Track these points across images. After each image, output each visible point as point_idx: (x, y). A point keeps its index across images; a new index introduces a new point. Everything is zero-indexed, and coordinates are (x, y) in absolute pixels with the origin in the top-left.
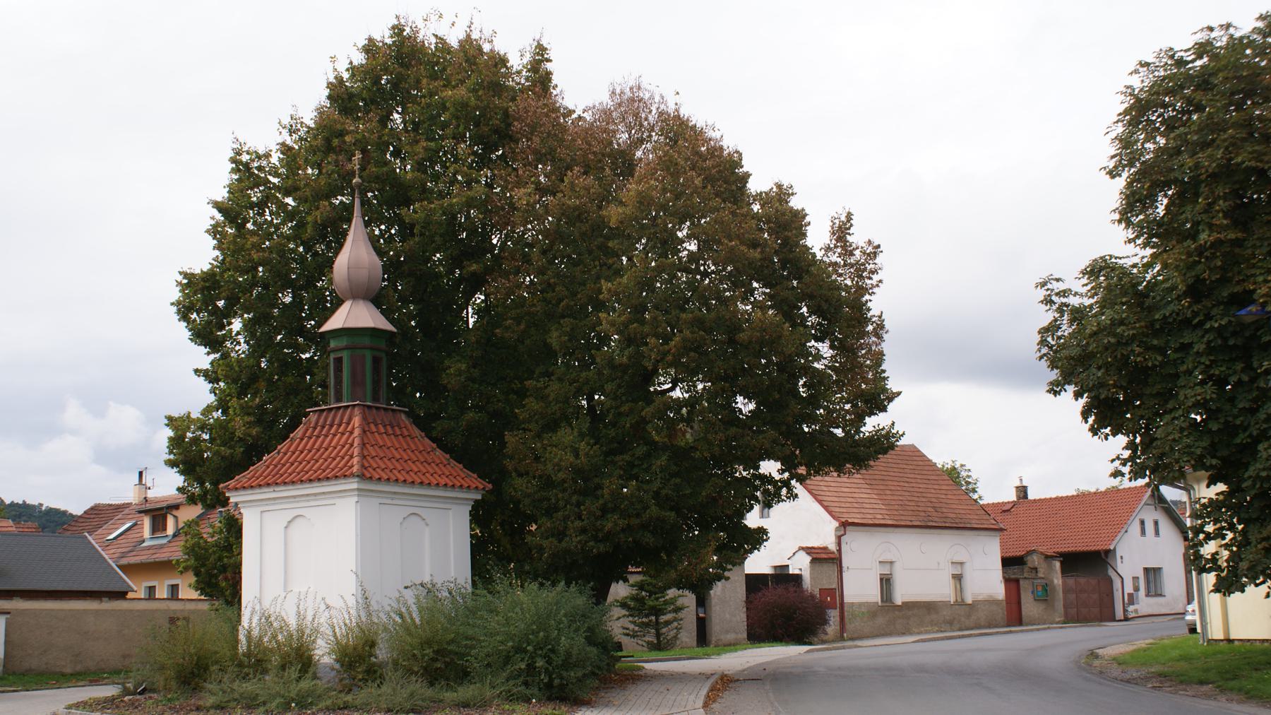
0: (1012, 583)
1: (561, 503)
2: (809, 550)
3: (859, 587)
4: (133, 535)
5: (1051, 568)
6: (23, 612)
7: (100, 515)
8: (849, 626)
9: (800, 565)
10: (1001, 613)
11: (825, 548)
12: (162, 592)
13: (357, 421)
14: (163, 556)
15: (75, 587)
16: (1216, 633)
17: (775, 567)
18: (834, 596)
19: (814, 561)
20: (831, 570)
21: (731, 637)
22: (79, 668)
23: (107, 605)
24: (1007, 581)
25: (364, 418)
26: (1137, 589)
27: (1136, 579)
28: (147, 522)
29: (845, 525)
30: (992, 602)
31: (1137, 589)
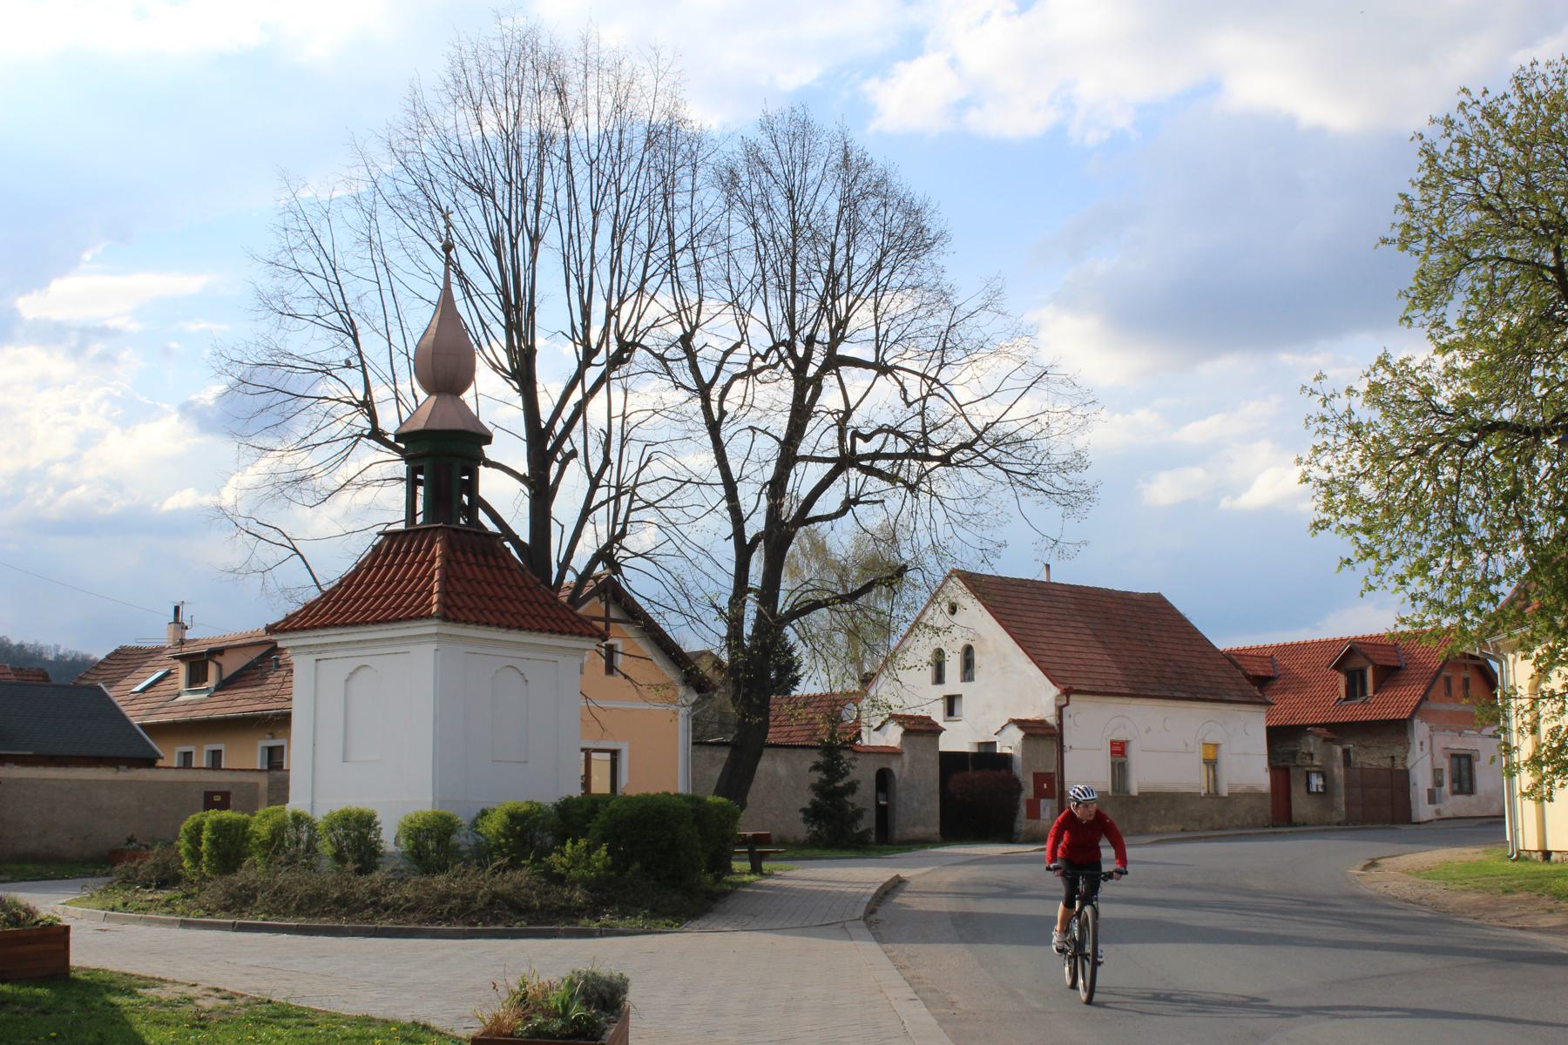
3: (1085, 774)
5: (1330, 756)
9: (1010, 743)
11: (1043, 722)
18: (1050, 784)
20: (1049, 748)
21: (919, 831)
24: (1274, 768)
26: (1439, 784)
29: (1067, 692)
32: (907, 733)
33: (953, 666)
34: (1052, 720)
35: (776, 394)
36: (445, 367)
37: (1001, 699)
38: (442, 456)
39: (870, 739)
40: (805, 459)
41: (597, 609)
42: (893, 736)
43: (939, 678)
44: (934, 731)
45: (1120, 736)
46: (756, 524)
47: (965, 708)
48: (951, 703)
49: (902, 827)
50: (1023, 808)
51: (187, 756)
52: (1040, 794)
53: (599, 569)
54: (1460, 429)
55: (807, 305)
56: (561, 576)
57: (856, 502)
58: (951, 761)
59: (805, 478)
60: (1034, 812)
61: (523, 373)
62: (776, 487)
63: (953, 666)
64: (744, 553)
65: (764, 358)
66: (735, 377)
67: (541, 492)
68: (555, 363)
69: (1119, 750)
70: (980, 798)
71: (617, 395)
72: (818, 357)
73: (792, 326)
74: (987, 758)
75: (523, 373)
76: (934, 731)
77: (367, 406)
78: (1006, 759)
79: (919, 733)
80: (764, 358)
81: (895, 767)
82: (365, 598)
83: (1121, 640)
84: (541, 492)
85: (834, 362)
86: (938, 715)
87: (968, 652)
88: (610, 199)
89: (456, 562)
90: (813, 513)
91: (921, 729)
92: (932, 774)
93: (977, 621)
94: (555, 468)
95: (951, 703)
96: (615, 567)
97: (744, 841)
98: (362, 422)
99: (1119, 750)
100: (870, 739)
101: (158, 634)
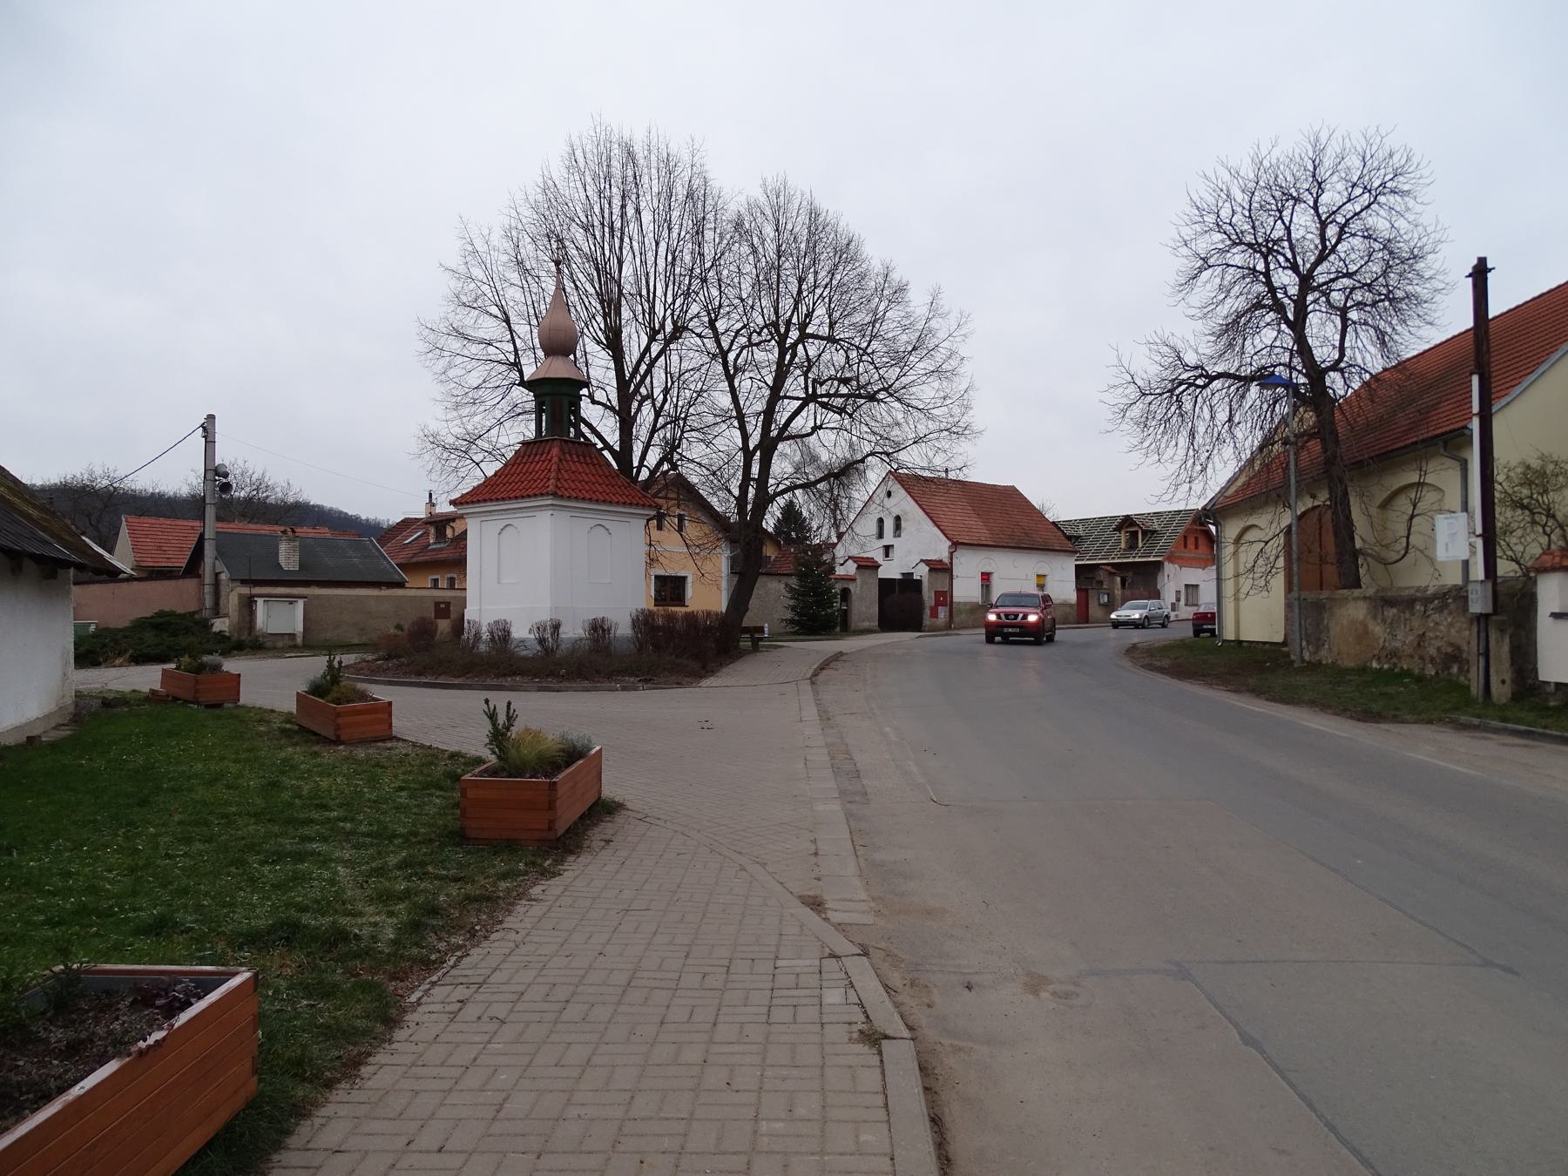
0: (1081, 590)
1: (1514, 525)
2: (927, 562)
3: (966, 589)
4: (422, 541)
5: (1113, 582)
6: (318, 596)
7: (407, 524)
8: (956, 619)
9: (921, 572)
10: (1074, 612)
11: (941, 561)
12: (443, 583)
13: (555, 451)
14: (442, 556)
15: (370, 579)
16: (1229, 634)
17: (1542, 457)
18: (944, 597)
19: (931, 570)
20: (945, 577)
21: (866, 624)
22: (364, 639)
23: (385, 592)
24: (1078, 590)
25: (561, 449)
26: (1178, 600)
27: (1178, 592)
28: (432, 530)
29: (956, 545)
30: (1065, 604)
31: (1178, 600)
32: (859, 567)
33: (889, 525)
34: (946, 560)
35: (767, 356)
36: (559, 345)
37: (915, 547)
38: (557, 398)
39: (840, 571)
40: (786, 397)
41: (667, 496)
42: (851, 568)
43: (880, 535)
44: (877, 567)
45: (987, 569)
46: (753, 442)
47: (895, 554)
48: (887, 549)
49: (856, 620)
50: (927, 611)
51: (436, 581)
52: (938, 603)
53: (666, 467)
54: (1197, 378)
55: (786, 304)
56: (639, 472)
57: (820, 427)
58: (886, 585)
59: (786, 408)
60: (934, 614)
61: (614, 344)
62: (769, 413)
63: (889, 525)
64: (748, 455)
65: (759, 334)
66: (743, 348)
67: (626, 423)
68: (634, 340)
69: (986, 577)
70: (903, 605)
71: (675, 358)
72: (794, 334)
73: (776, 312)
74: (909, 584)
75: (614, 344)
76: (877, 567)
77: (516, 365)
78: (919, 582)
79: (866, 567)
80: (759, 334)
81: (852, 587)
82: (512, 485)
83: (1002, 518)
84: (626, 423)
85: (804, 337)
86: (878, 556)
87: (898, 519)
88: (665, 234)
89: (559, 461)
90: (658, 405)
91: (868, 566)
92: (874, 593)
93: (902, 502)
94: (635, 404)
95: (887, 549)
96: (674, 466)
97: (746, 630)
98: (515, 375)
99: (986, 577)
100: (840, 571)
101: (420, 512)
